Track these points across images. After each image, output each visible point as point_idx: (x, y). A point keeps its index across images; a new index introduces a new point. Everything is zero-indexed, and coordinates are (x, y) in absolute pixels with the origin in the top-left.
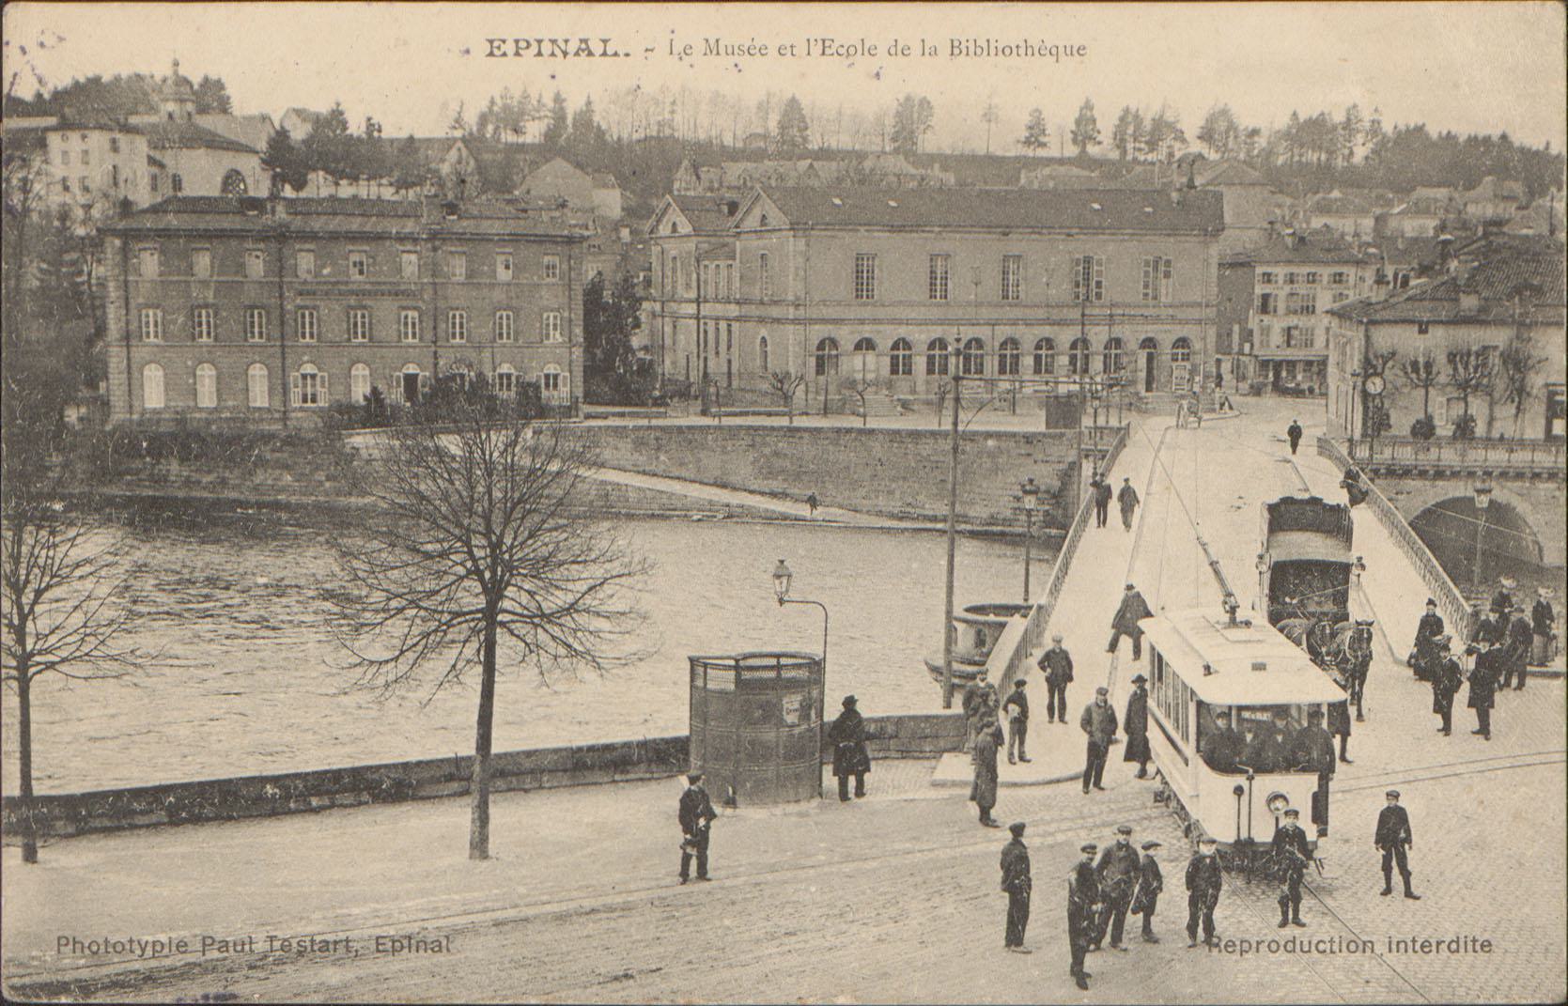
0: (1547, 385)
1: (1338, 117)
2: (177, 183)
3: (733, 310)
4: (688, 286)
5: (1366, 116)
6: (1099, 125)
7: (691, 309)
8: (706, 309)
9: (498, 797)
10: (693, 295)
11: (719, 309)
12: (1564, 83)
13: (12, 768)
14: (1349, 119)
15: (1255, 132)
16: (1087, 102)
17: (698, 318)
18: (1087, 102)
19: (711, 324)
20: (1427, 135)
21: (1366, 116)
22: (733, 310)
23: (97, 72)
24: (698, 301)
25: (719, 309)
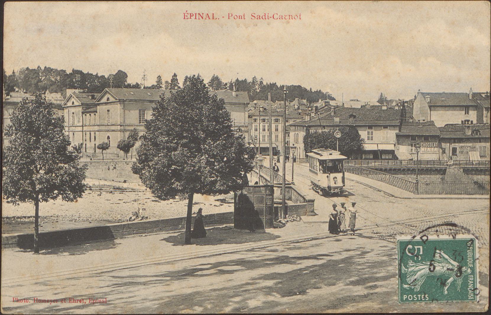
0: (250, 219)
1: (250, 80)
2: (62, 94)
3: (96, 128)
4: (79, 122)
5: (258, 79)
6: (179, 82)
7: (80, 129)
8: (85, 128)
9: (231, 213)
10: (81, 124)
11: (91, 128)
12: (22, 2)
13: (429, 117)
14: (253, 82)
15: (226, 84)
16: (175, 74)
17: (83, 131)
18: (175, 74)
19: (88, 133)
20: (277, 86)
21: (258, 79)
22: (96, 128)
23: (366, 101)
24: (83, 126)
25: (91, 128)
